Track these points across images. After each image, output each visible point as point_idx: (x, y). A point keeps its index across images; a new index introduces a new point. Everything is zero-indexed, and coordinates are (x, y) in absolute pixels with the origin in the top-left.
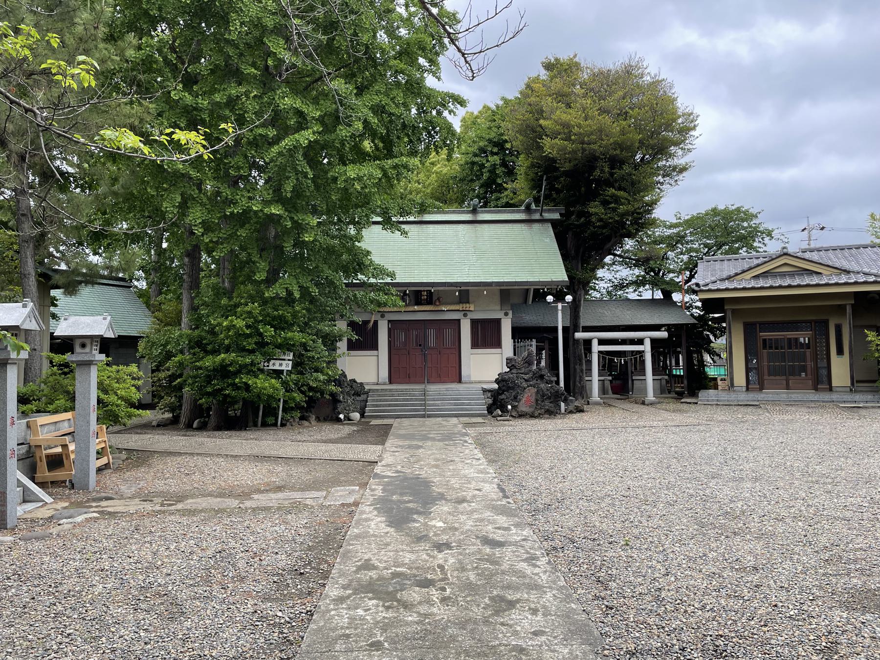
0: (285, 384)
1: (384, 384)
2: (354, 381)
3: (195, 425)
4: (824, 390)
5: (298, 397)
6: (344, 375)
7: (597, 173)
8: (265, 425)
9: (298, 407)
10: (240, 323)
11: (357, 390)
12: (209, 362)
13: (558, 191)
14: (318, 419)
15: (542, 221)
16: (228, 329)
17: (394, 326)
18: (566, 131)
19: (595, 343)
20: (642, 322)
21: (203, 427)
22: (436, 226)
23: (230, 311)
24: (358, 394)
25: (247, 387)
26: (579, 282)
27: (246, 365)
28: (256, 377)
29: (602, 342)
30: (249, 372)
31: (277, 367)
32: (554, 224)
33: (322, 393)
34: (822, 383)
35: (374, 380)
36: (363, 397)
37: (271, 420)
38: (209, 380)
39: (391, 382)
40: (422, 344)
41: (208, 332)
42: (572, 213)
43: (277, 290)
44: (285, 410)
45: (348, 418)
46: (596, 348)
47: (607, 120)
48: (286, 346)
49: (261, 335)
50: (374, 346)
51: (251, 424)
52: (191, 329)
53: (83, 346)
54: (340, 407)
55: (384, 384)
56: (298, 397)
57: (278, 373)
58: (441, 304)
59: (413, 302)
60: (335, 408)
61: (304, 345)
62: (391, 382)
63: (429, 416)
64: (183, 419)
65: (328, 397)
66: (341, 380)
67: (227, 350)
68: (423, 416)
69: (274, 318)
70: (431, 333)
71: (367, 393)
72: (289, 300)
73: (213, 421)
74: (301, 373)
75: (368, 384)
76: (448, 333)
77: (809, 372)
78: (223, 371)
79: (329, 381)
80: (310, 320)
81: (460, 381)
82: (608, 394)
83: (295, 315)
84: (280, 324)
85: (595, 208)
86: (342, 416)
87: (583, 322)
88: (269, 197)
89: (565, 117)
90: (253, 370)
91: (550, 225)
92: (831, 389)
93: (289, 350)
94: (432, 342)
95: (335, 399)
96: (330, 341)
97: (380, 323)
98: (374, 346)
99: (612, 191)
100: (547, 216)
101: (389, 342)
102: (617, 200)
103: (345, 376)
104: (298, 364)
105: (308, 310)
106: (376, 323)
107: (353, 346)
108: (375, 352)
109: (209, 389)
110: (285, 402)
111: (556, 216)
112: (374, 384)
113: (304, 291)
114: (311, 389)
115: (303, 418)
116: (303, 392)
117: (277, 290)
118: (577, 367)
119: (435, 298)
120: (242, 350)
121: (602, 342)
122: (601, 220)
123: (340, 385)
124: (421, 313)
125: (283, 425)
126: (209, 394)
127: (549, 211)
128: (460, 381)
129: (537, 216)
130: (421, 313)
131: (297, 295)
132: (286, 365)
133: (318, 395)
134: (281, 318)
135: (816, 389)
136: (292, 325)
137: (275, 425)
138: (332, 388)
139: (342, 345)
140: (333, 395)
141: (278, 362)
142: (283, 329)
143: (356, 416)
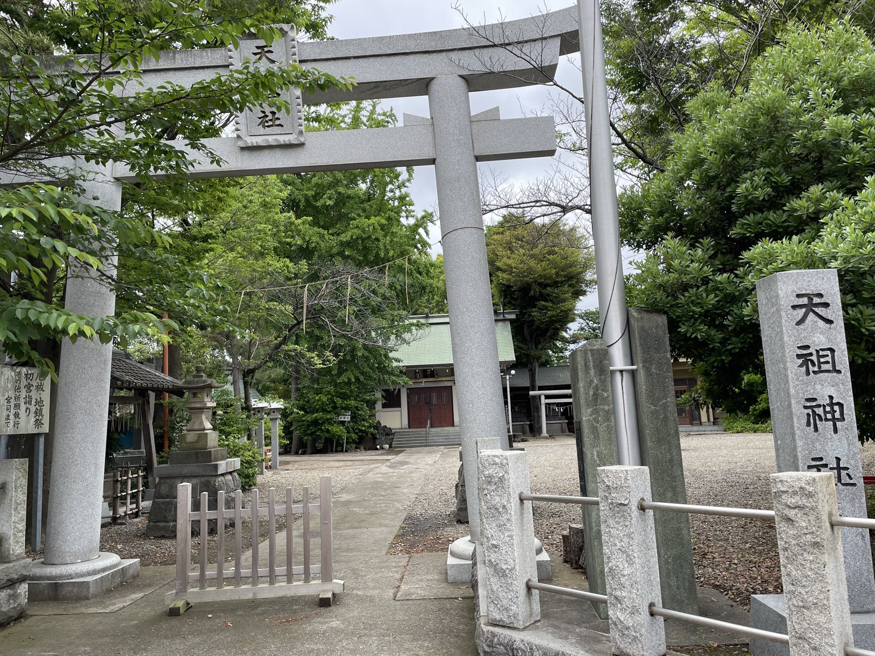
0: (347, 428)
1: (406, 429)
2: (385, 426)
3: (300, 452)
4: (696, 425)
5: (354, 436)
6: (379, 422)
7: (532, 293)
8: (337, 451)
9: (354, 442)
10: (325, 399)
11: (388, 433)
12: (309, 418)
13: (516, 299)
14: (365, 449)
15: (504, 320)
16: (318, 401)
17: (411, 392)
18: (509, 270)
19: (543, 397)
20: (547, 384)
21: (304, 453)
22: (437, 326)
23: (318, 392)
24: (388, 435)
25: (328, 431)
26: (533, 358)
27: (327, 419)
28: (332, 425)
29: (547, 397)
30: (330, 424)
31: (343, 419)
32: (512, 321)
33: (367, 434)
34: (696, 420)
35: (400, 427)
36: (391, 437)
37: (339, 448)
38: (308, 426)
39: (410, 427)
40: (429, 403)
41: (306, 402)
42: (525, 313)
43: (343, 378)
44: (347, 443)
45: (382, 448)
46: (544, 401)
47: (532, 263)
48: (346, 408)
49: (335, 403)
50: (399, 405)
51: (329, 450)
52: (297, 400)
53: (274, 412)
54: (377, 442)
55: (406, 429)
56: (354, 436)
57: (343, 423)
58: (439, 377)
59: (422, 376)
60: (375, 443)
61: (356, 408)
62: (410, 427)
63: (429, 446)
64: (293, 449)
65: (370, 436)
66: (377, 426)
67: (317, 411)
68: (426, 446)
69: (341, 394)
70: (434, 396)
71: (393, 434)
72: (349, 383)
73: (309, 449)
74: (356, 423)
75: (395, 429)
76: (445, 395)
77: (687, 412)
78: (315, 423)
79: (370, 427)
80: (359, 393)
81: (453, 425)
82: (565, 432)
83: (351, 391)
84: (344, 397)
85: (535, 313)
86: (378, 447)
87: (538, 383)
88: (404, 562)
89: (510, 262)
90: (329, 421)
91: (509, 323)
92: (701, 424)
93: (349, 410)
94: (434, 401)
95: (374, 438)
96: (371, 404)
97: (402, 390)
98: (399, 405)
99: (543, 303)
100: (508, 316)
101: (408, 402)
102: (546, 308)
103: (380, 424)
104: (353, 417)
105: (358, 388)
106: (399, 390)
107: (384, 406)
108: (399, 409)
109: (309, 432)
110: (347, 439)
111: (513, 317)
112: (399, 429)
113: (357, 379)
114: (361, 431)
115: (356, 448)
116: (356, 433)
117: (343, 378)
118: (536, 414)
119: (435, 373)
120: (324, 411)
121: (547, 397)
122: (539, 320)
123: (377, 429)
124: (424, 383)
125: (346, 451)
126: (308, 435)
127: (509, 313)
128: (453, 425)
129: (501, 317)
130: (424, 383)
131: (353, 380)
132: (347, 418)
133: (365, 434)
134: (344, 393)
135: (692, 424)
136: (350, 397)
137: (342, 451)
138: (372, 430)
139: (379, 406)
140: (372, 434)
141: (343, 417)
142: (345, 399)
143: (387, 446)
